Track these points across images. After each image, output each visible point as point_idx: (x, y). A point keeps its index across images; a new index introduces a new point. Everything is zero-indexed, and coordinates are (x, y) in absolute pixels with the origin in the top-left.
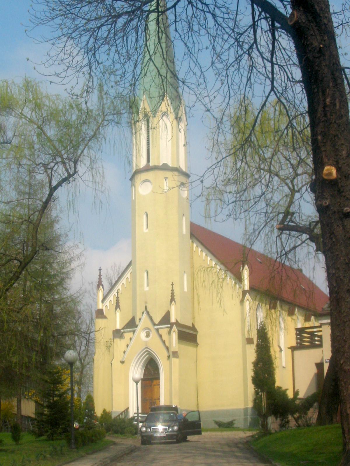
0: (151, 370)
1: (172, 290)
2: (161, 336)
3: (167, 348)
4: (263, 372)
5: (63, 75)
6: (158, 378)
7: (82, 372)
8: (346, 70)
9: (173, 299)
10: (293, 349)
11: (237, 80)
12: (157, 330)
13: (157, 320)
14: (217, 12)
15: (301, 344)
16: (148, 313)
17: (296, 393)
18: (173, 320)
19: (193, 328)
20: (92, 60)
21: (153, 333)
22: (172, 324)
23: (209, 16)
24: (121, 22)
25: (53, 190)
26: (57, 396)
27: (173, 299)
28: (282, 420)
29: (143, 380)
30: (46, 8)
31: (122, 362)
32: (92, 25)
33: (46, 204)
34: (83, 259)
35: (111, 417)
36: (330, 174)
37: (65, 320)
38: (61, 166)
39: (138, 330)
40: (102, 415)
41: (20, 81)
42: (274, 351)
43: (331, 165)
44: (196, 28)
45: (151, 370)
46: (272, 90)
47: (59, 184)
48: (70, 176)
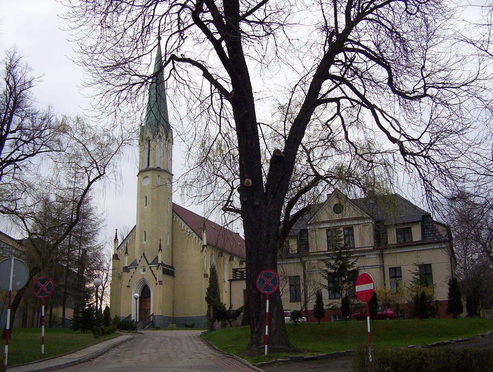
0: (145, 293)
1: (160, 244)
2: (152, 271)
3: (156, 279)
4: (213, 293)
5: (99, 117)
6: (150, 297)
7: (103, 292)
8: (261, 125)
9: (160, 249)
10: (230, 281)
11: (200, 124)
12: (150, 267)
13: (150, 262)
14: (191, 85)
15: (235, 278)
16: (145, 257)
17: (231, 307)
18: (160, 262)
19: (172, 267)
20: (117, 109)
21: (147, 269)
22: (159, 264)
23: (186, 87)
24: (135, 88)
25: (90, 183)
26: (88, 306)
27: (160, 249)
28: (222, 323)
29: (140, 298)
30: (91, 77)
31: (128, 287)
32: (118, 89)
33: (86, 191)
34: (105, 223)
35: (120, 320)
36: (248, 183)
37: (83, 224)
38: (96, 170)
39: (138, 267)
40: (115, 319)
41: (74, 117)
42: (220, 280)
43: (249, 178)
44: (178, 93)
45: (145, 293)
46: (220, 132)
47: (94, 180)
48: (101, 175)
